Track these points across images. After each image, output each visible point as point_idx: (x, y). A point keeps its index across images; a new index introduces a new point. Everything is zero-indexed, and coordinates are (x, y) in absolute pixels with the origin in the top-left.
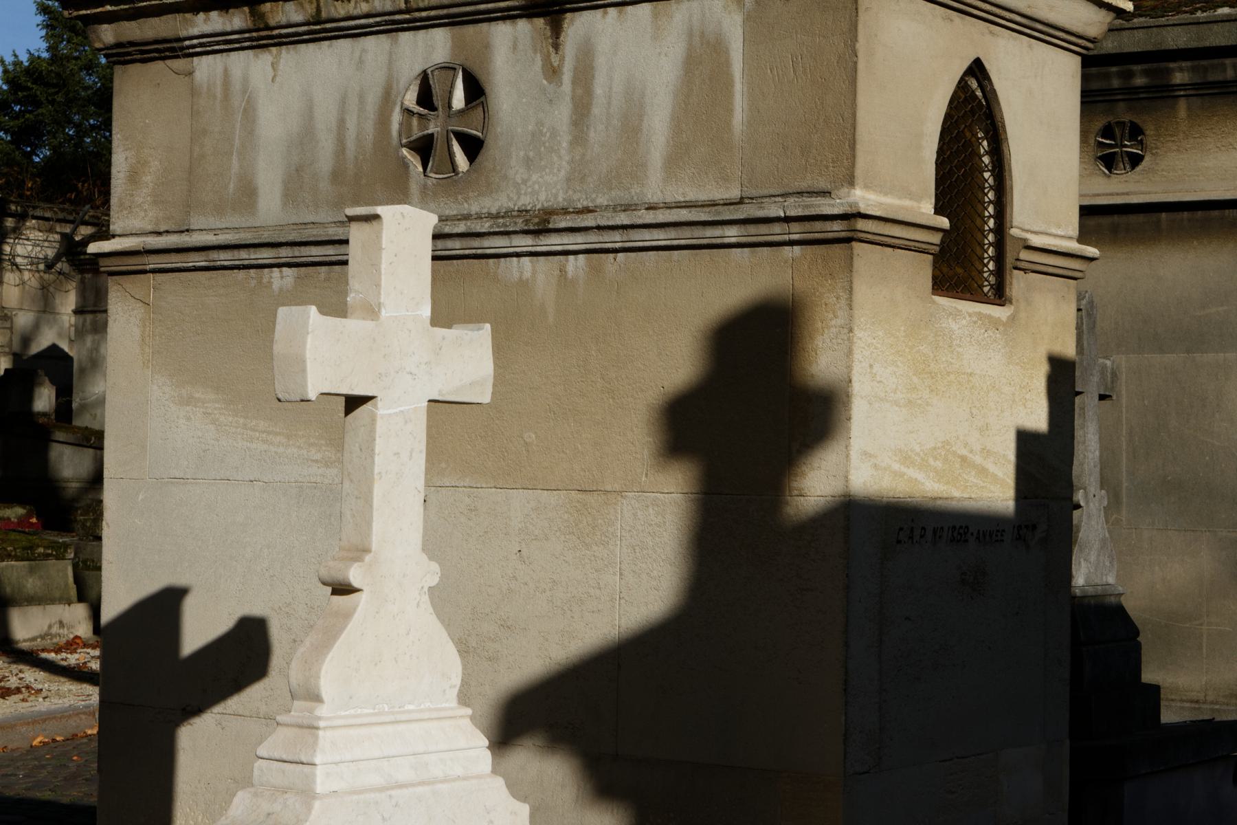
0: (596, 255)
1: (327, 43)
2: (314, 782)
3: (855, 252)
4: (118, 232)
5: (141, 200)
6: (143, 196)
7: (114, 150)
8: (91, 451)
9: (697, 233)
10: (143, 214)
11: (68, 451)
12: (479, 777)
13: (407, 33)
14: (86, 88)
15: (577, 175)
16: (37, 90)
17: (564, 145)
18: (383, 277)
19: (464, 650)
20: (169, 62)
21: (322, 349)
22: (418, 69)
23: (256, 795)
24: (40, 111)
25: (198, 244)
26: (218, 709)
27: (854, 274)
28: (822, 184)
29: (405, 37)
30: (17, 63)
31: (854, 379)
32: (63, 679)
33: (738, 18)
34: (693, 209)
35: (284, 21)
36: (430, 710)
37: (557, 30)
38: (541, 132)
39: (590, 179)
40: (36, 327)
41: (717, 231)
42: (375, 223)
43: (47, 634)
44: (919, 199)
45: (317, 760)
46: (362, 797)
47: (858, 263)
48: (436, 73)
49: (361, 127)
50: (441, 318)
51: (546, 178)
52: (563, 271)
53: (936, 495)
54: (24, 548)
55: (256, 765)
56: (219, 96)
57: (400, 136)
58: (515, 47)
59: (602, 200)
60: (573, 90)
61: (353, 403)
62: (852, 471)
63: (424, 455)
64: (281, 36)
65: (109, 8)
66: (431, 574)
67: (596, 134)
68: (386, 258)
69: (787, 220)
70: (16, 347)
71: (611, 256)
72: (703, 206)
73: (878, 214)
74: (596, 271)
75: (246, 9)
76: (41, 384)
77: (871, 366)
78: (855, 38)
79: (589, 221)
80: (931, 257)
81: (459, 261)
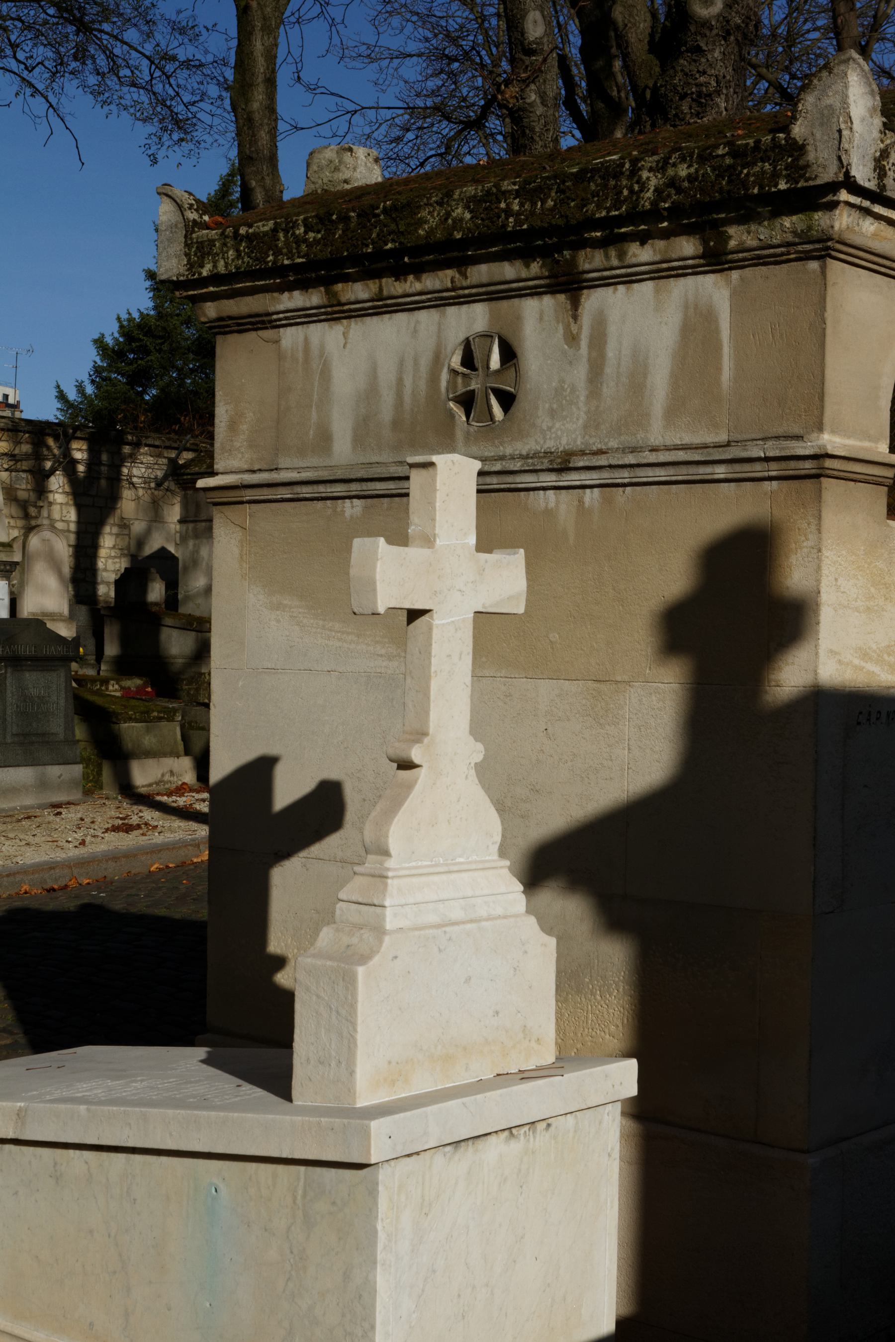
0: (608, 489)
1: (387, 316)
2: (384, 920)
3: (823, 486)
4: (221, 471)
5: (239, 445)
6: (240, 441)
7: (217, 404)
8: (194, 633)
9: (691, 471)
10: (240, 456)
11: (175, 633)
12: (516, 916)
13: (453, 307)
14: (187, 339)
15: (593, 423)
16: (148, 341)
17: (582, 398)
18: (437, 513)
19: (501, 808)
20: (260, 333)
21: (390, 574)
22: (462, 337)
23: (337, 930)
24: (149, 358)
25: (285, 481)
26: (303, 854)
27: (823, 504)
28: (796, 430)
29: (451, 311)
30: (131, 320)
31: (823, 590)
32: (174, 818)
33: (726, 293)
34: (689, 451)
35: (353, 298)
36: (476, 862)
37: (575, 304)
38: (563, 387)
39: (603, 427)
40: (148, 532)
41: (708, 469)
42: (430, 469)
43: (160, 781)
44: (876, 440)
45: (387, 903)
46: (422, 932)
47: (827, 496)
48: (477, 340)
49: (415, 384)
50: (485, 545)
51: (567, 426)
52: (581, 501)
53: (889, 684)
54: (142, 713)
55: (338, 906)
56: (301, 360)
57: (447, 391)
58: (541, 319)
59: (613, 444)
60: (589, 353)
61: (414, 615)
62: (821, 666)
63: (471, 656)
64: (350, 310)
65: (211, 289)
66: (476, 752)
67: (609, 389)
68: (440, 496)
69: (767, 459)
70: (133, 549)
71: (621, 489)
72: (696, 448)
73: (843, 454)
74: (608, 502)
75: (322, 289)
76: (153, 580)
77: (836, 580)
78: (823, 308)
79: (602, 461)
80: (886, 489)
81: (496, 494)
